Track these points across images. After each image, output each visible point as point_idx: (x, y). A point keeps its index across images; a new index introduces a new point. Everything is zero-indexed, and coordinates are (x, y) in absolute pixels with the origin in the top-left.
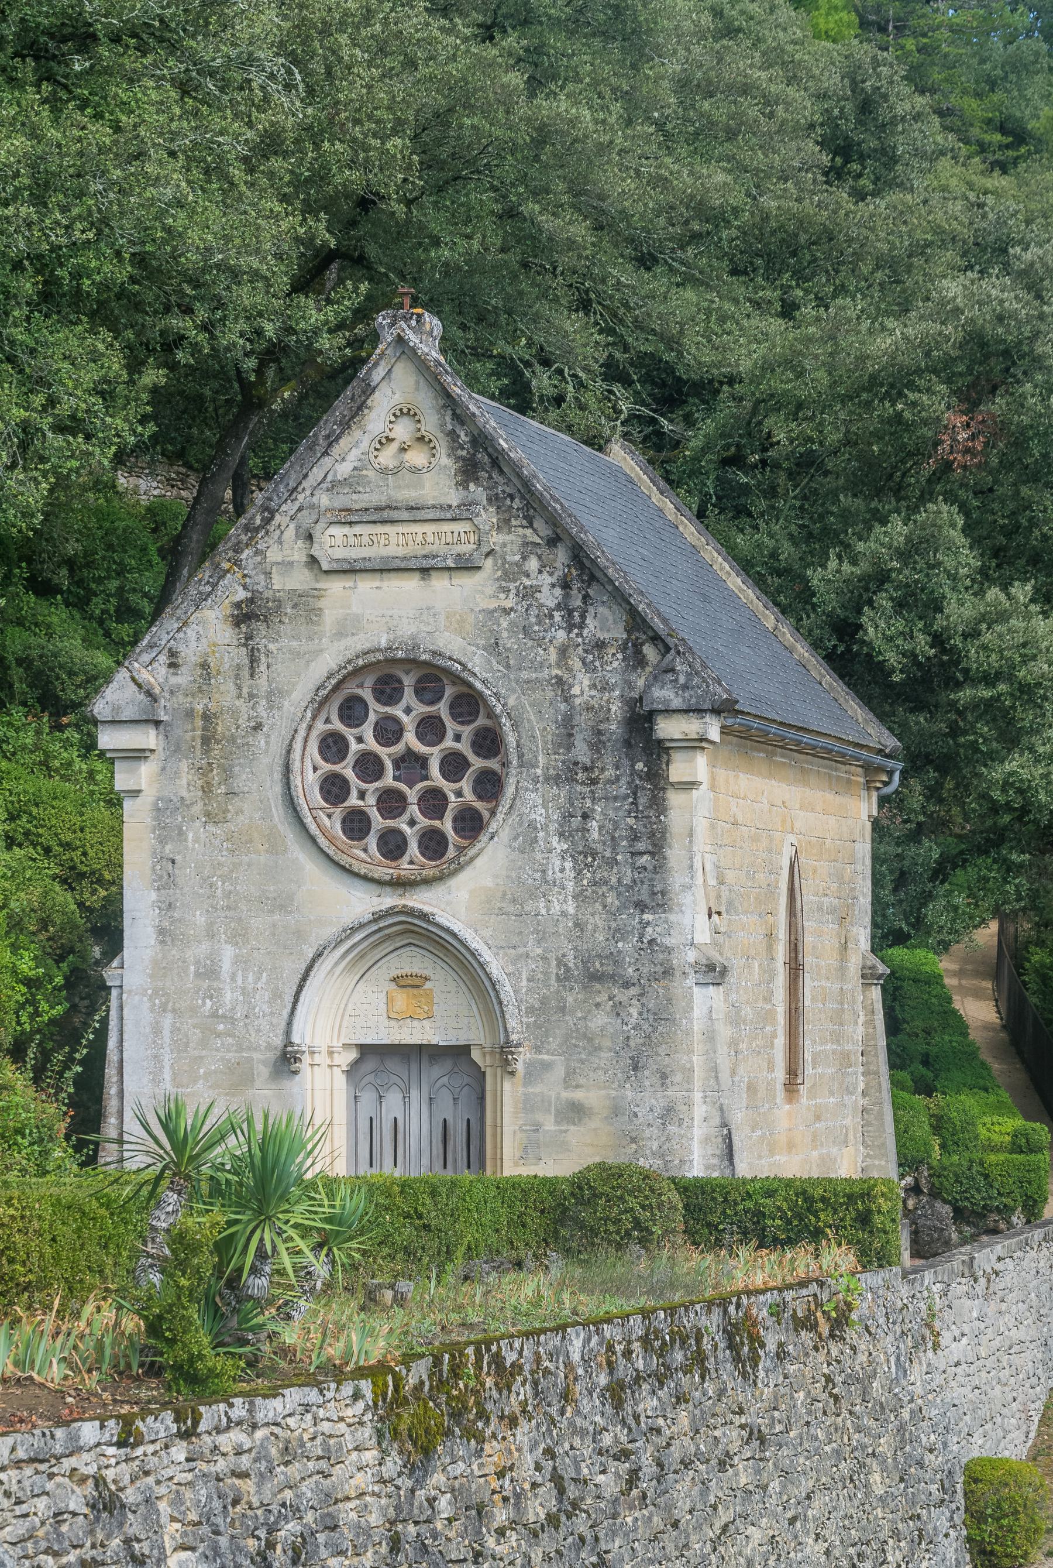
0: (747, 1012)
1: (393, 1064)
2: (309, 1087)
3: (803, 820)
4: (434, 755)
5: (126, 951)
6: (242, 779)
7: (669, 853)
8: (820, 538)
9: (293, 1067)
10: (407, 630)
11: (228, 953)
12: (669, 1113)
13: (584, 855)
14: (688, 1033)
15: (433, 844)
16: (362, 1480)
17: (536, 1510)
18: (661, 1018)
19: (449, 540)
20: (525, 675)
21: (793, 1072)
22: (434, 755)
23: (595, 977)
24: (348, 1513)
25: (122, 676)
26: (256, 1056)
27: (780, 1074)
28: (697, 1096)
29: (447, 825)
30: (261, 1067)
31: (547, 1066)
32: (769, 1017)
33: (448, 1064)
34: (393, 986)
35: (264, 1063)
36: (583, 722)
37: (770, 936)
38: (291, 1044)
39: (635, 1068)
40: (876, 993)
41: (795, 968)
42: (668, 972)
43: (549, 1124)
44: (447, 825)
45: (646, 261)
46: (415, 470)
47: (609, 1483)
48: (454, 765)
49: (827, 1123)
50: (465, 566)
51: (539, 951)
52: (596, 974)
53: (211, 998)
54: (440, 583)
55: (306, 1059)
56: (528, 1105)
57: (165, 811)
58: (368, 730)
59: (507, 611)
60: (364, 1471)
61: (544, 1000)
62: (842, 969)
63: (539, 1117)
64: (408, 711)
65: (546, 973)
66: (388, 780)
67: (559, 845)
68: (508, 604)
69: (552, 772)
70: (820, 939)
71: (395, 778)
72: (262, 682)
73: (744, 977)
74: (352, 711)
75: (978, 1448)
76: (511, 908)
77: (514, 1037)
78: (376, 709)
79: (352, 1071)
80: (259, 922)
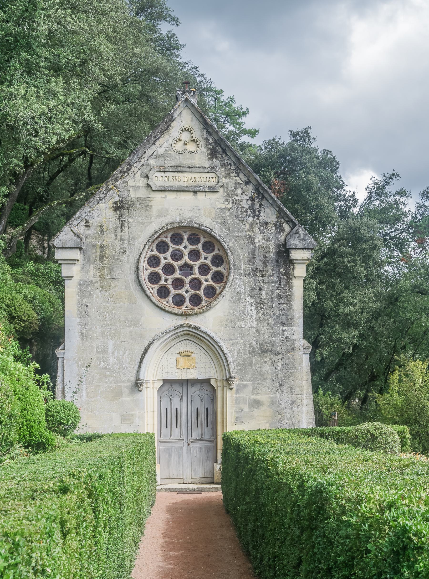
2: (146, 396)
6: (117, 273)
9: (140, 389)
12: (293, 403)
13: (260, 305)
15: (196, 300)
23: (264, 351)
25: (66, 229)
26: (123, 385)
30: (126, 389)
31: (245, 386)
33: (199, 386)
35: (127, 387)
36: (259, 253)
38: (140, 380)
43: (246, 408)
51: (242, 341)
55: (144, 385)
56: (238, 401)
57: (84, 286)
61: (244, 361)
63: (242, 406)
74: (162, 247)
76: (231, 325)
77: (233, 375)
78: (172, 247)
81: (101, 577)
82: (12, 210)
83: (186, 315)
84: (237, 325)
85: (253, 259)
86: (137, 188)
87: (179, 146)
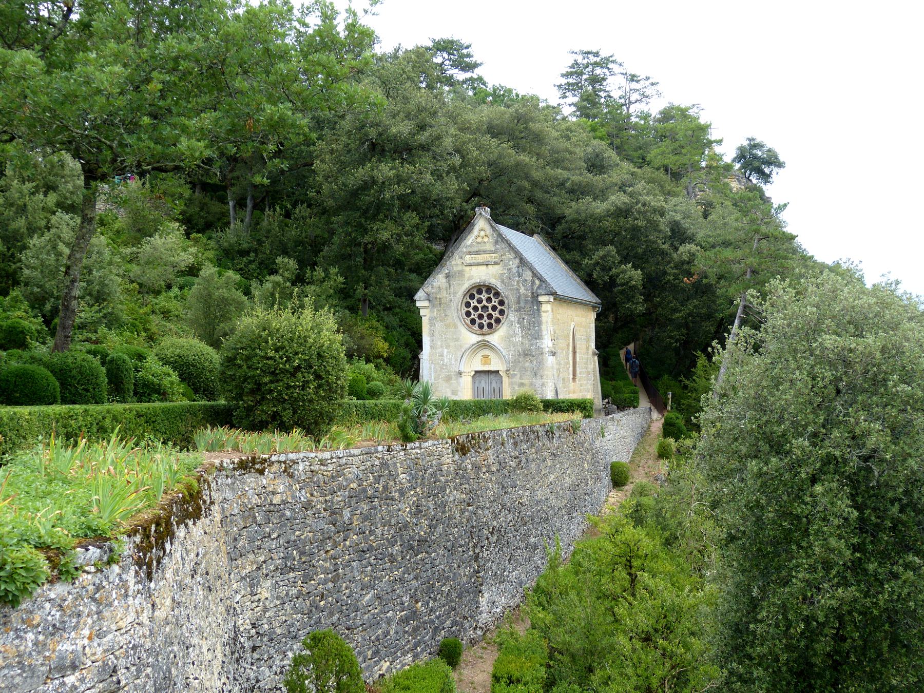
0: (562, 362)
1: (482, 375)
3: (576, 319)
4: (490, 306)
6: (448, 313)
8: (584, 253)
10: (483, 278)
11: (446, 350)
12: (543, 385)
13: (522, 327)
15: (490, 326)
16: (448, 461)
17: (494, 469)
18: (541, 363)
21: (574, 375)
23: (526, 355)
24: (445, 468)
25: (421, 290)
27: (571, 376)
29: (493, 321)
32: (568, 363)
36: (522, 298)
37: (568, 345)
40: (596, 358)
41: (574, 352)
42: (542, 353)
44: (493, 321)
45: (547, 192)
47: (513, 464)
48: (494, 308)
49: (586, 385)
50: (495, 263)
52: (527, 354)
57: (432, 320)
58: (475, 301)
60: (449, 459)
62: (587, 353)
66: (480, 312)
67: (518, 326)
70: (581, 346)
73: (561, 355)
74: (472, 297)
75: (614, 459)
78: (477, 296)
79: (473, 377)
80: (452, 344)
81: (230, 691)
82: (633, 78)
83: (483, 335)
85: (518, 302)
86: (457, 265)
87: (479, 240)
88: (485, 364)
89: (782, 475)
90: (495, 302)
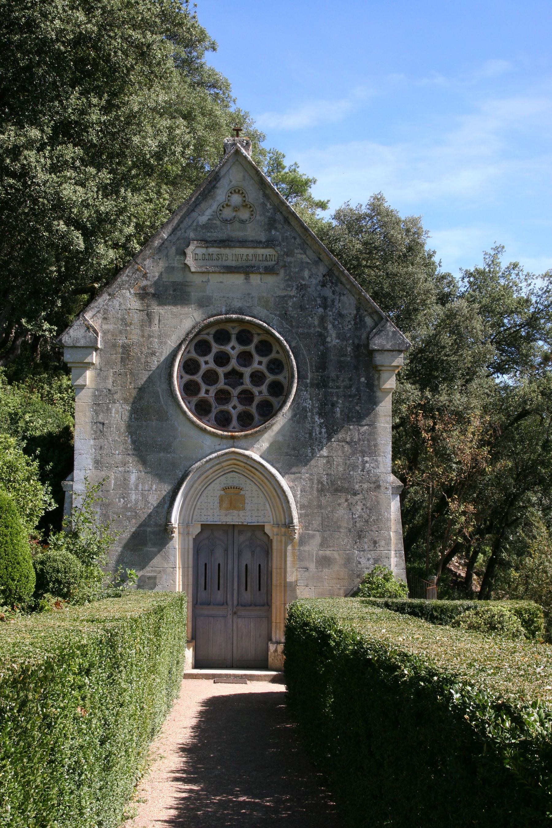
4: (247, 372)
5: (75, 472)
7: (378, 425)
14: (389, 520)
19: (261, 258)
20: (300, 330)
22: (247, 372)
23: (337, 490)
26: (149, 529)
28: (393, 553)
34: (222, 492)
36: (333, 357)
39: (360, 537)
44: (253, 409)
46: (242, 222)
50: (270, 271)
53: (123, 498)
54: (255, 279)
59: (291, 297)
64: (233, 349)
65: (311, 487)
68: (293, 293)
69: (315, 382)
71: (225, 384)
72: (155, 328)
74: (244, 337)
76: (293, 453)
78: (215, 348)
84: (301, 453)
87: (228, 213)
88: (207, 365)
89: (196, 168)
90: (259, 363)
